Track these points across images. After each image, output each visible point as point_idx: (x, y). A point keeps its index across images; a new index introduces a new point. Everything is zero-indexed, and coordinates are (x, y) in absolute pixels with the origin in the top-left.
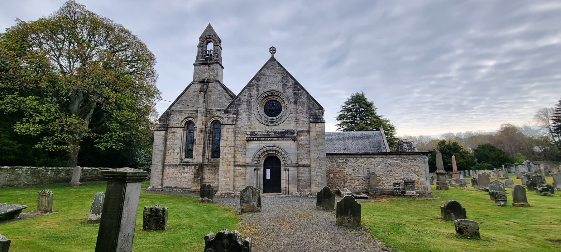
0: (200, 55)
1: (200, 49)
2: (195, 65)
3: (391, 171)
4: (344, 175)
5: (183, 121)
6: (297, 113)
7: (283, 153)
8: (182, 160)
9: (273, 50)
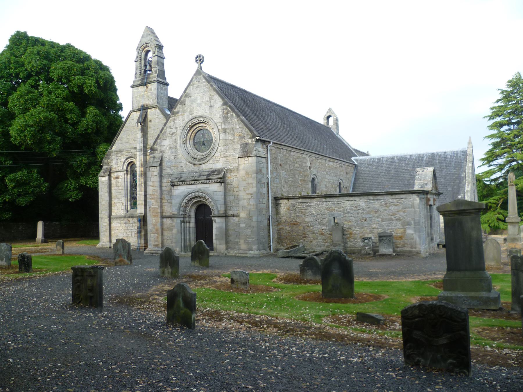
0: (138, 72)
1: (138, 63)
2: (132, 87)
3: (366, 220)
4: (304, 227)
5: (124, 162)
6: (226, 145)
7: (210, 200)
8: (127, 211)
9: (200, 59)
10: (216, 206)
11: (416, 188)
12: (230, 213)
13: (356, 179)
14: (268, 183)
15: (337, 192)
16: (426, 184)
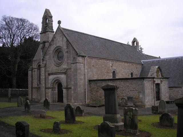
10: (64, 84)
11: (149, 76)
12: (69, 87)
13: (142, 71)
14: (85, 74)
15: (130, 77)
16: (153, 74)
